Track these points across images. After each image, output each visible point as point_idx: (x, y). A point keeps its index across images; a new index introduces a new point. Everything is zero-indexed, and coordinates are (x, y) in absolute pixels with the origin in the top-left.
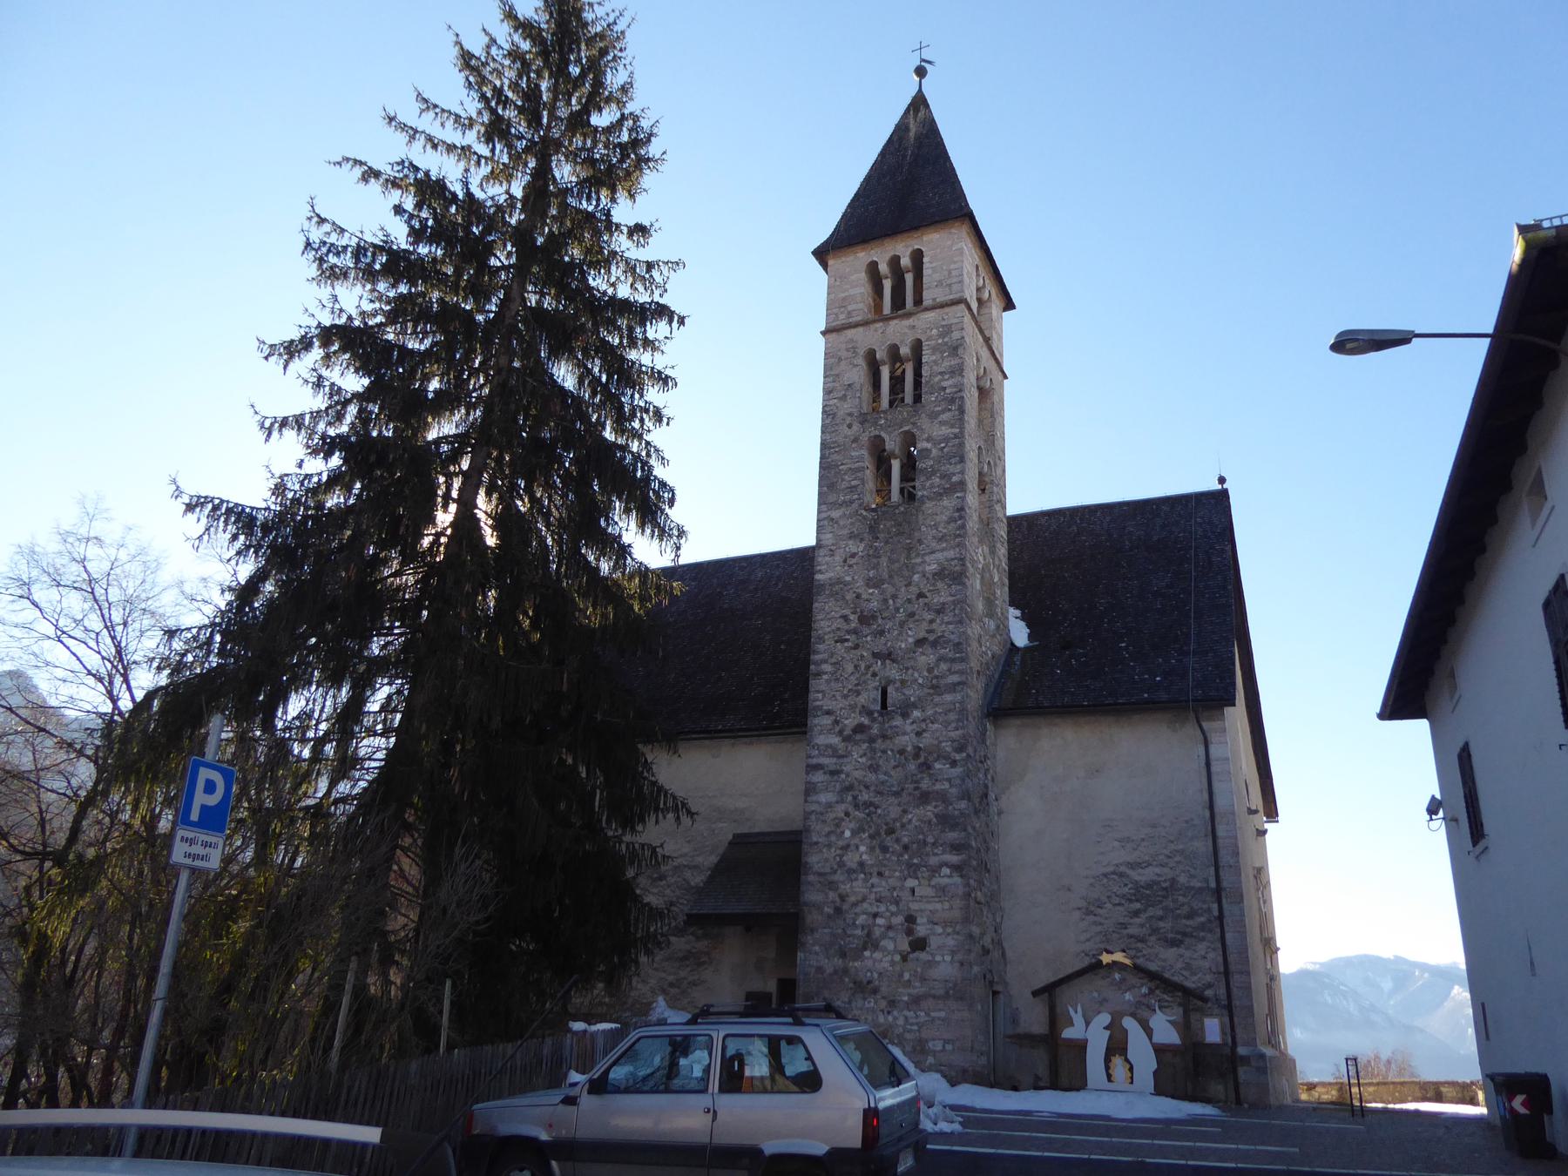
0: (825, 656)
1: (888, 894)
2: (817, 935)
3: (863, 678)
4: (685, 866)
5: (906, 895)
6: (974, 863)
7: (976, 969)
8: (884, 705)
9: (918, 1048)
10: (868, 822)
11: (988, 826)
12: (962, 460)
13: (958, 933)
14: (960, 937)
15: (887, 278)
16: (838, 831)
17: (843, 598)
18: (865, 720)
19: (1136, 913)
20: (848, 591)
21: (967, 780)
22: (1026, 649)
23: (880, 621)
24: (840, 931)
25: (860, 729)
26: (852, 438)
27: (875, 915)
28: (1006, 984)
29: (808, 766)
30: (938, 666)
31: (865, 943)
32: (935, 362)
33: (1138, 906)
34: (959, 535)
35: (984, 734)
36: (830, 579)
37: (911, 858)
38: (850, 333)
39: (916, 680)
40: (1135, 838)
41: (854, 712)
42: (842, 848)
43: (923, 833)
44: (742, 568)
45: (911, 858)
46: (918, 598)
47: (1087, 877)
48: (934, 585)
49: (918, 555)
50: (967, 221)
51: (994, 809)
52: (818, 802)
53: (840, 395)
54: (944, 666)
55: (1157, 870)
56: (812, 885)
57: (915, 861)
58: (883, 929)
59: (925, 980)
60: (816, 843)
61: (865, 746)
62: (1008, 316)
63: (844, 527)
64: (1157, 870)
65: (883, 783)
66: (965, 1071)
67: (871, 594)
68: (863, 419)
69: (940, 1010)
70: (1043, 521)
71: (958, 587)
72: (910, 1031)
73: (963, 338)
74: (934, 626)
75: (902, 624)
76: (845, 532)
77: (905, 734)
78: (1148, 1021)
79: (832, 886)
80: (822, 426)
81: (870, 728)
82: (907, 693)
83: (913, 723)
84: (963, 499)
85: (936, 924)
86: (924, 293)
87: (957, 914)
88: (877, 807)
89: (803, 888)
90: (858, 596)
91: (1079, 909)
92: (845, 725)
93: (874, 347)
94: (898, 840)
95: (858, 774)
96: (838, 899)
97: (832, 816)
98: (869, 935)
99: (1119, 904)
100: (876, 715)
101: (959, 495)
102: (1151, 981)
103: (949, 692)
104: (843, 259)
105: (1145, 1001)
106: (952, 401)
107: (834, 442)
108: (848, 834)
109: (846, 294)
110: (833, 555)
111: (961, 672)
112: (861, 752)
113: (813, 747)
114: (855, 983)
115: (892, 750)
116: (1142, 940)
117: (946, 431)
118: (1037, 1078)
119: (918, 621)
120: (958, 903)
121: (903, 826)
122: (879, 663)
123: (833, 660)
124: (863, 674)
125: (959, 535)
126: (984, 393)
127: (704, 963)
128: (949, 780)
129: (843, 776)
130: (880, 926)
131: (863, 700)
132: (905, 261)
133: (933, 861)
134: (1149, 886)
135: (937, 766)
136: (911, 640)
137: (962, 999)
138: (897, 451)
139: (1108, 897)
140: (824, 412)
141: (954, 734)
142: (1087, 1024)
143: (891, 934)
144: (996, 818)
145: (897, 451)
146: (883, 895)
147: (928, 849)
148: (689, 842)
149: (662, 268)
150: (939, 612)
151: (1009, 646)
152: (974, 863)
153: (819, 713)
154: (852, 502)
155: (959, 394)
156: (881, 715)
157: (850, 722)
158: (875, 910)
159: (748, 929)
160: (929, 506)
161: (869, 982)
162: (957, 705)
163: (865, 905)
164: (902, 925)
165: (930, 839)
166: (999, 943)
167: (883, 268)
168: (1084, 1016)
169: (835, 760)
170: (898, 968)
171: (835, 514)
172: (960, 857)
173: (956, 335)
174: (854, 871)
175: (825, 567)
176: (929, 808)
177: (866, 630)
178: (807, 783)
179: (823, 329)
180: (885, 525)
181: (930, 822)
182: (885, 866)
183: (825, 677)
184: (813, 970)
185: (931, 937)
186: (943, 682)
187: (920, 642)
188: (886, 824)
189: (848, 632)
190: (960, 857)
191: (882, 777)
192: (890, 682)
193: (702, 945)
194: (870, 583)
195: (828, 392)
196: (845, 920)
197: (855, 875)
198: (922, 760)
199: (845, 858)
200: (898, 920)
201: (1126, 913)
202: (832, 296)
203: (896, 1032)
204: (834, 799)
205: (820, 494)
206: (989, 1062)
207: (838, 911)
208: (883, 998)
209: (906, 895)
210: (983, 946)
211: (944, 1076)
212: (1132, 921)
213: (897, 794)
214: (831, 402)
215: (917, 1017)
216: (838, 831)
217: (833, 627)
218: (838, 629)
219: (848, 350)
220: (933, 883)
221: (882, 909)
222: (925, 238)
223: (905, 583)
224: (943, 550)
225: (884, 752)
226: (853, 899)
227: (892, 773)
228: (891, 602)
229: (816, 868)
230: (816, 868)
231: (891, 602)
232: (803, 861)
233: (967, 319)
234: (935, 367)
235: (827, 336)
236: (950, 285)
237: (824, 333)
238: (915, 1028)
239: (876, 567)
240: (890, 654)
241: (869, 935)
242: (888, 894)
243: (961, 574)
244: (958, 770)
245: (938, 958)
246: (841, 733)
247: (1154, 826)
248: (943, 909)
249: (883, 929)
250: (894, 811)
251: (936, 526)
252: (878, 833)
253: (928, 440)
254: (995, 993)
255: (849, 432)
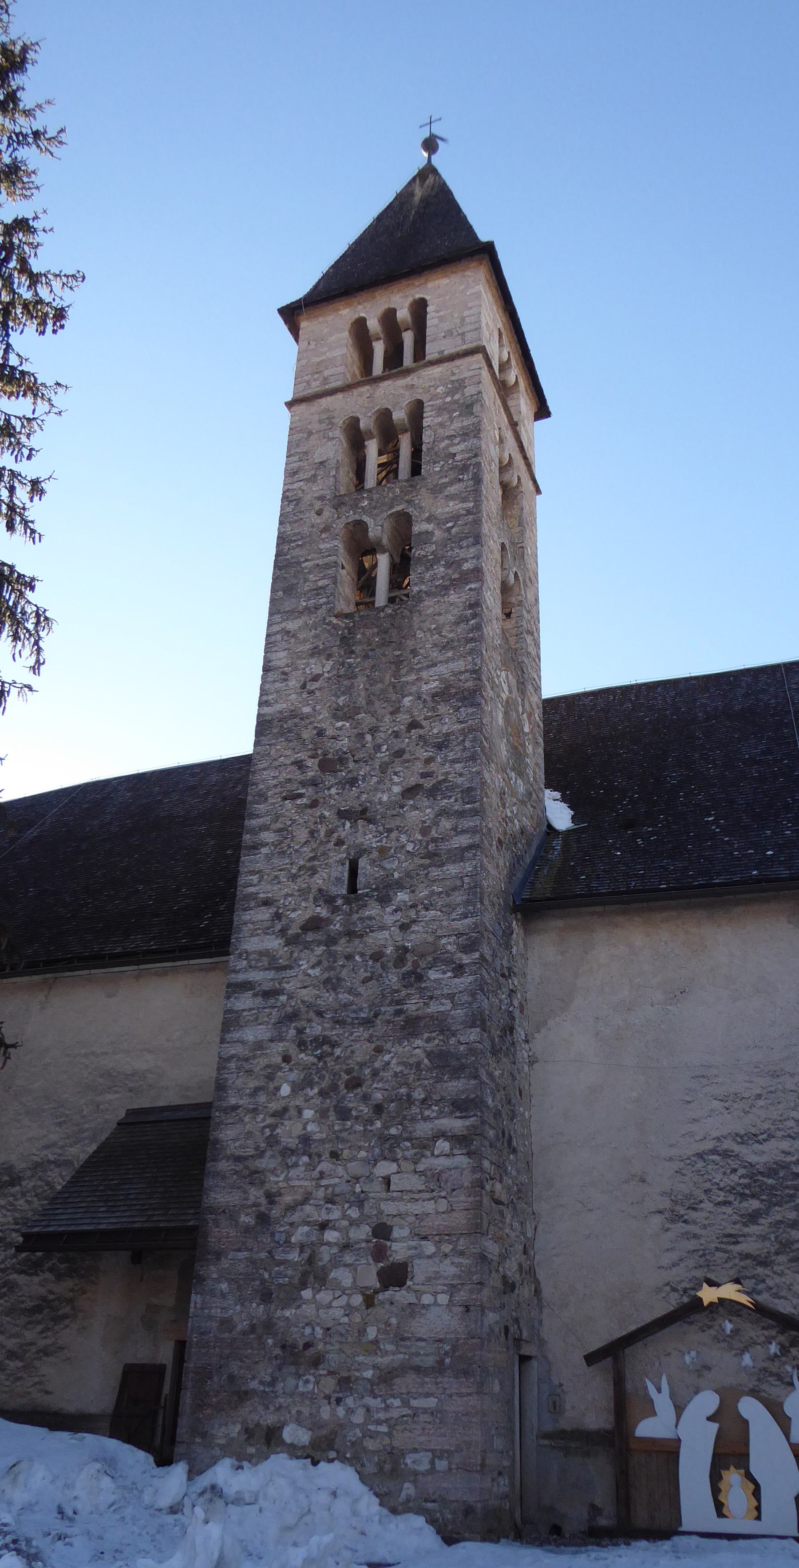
0: (266, 820)
1: (346, 1188)
2: (225, 1263)
3: (322, 849)
4: (49, 1162)
5: (376, 1189)
6: (491, 1133)
7: (492, 1317)
8: (353, 888)
9: (388, 1467)
10: (319, 1071)
11: (514, 1078)
12: (478, 540)
13: (462, 1254)
14: (465, 1261)
15: (378, 339)
16: (272, 1086)
17: (299, 737)
18: (323, 912)
19: (753, 1217)
20: (306, 727)
21: (480, 996)
22: (568, 832)
23: (351, 765)
24: (263, 1255)
25: (314, 924)
26: (322, 526)
27: (324, 1226)
28: (542, 1343)
29: (229, 985)
30: (436, 824)
31: (305, 1274)
32: (441, 425)
33: (755, 1204)
34: (472, 640)
35: (508, 933)
36: (281, 712)
37: (386, 1127)
38: (325, 402)
39: (403, 846)
40: (746, 1095)
41: (306, 900)
42: (274, 1115)
43: (407, 1084)
44: (193, 775)
45: (386, 1127)
46: (409, 730)
47: (671, 1159)
48: (434, 709)
49: (411, 670)
50: (486, 262)
51: (523, 1054)
52: (243, 1042)
53: (307, 475)
54: (446, 824)
55: (785, 1145)
56: (224, 1177)
57: (393, 1131)
58: (335, 1250)
59: (403, 1339)
60: (235, 1108)
61: (320, 950)
62: (538, 497)
63: (305, 640)
64: (785, 1145)
65: (345, 1006)
66: (468, 1510)
67: (340, 729)
68: (338, 503)
69: (428, 1395)
70: (587, 701)
71: (470, 710)
72: (373, 1435)
73: (480, 393)
74: (433, 767)
75: (384, 768)
76: (308, 646)
77: (382, 928)
78: (781, 1405)
79: (255, 1177)
80: (281, 515)
81: (328, 921)
82: (387, 866)
83: (396, 911)
84: (479, 591)
85: (425, 1238)
86: (428, 347)
87: (459, 1219)
88: (334, 1045)
89: (209, 1182)
90: (321, 733)
91: (660, 1212)
92: (292, 921)
93: (358, 415)
94: (366, 1098)
95: (306, 994)
96: (263, 1201)
97: (262, 1062)
98: (310, 1261)
99: (726, 1203)
100: (339, 902)
101: (473, 586)
102: (782, 1332)
103: (454, 862)
104: (321, 319)
105: (774, 1367)
106: (464, 469)
107: (295, 535)
108: (285, 1090)
109: (323, 357)
110: (286, 680)
111: (473, 831)
112: (314, 960)
113: (240, 955)
114: (283, 1347)
115: (362, 955)
116: (764, 1263)
117: (454, 506)
118: (270, 661)
119: (408, 761)
120: (462, 1199)
121: (375, 1073)
122: (348, 824)
123: (279, 825)
124: (321, 843)
125: (472, 640)
126: (509, 493)
127: (65, 1317)
128: (451, 997)
129: (283, 998)
130: (329, 1244)
131: (320, 882)
132: (403, 314)
133: (423, 1129)
134: (771, 1172)
135: (433, 975)
136: (397, 789)
137: (466, 1373)
138: (385, 541)
139: (707, 1191)
140: (285, 498)
141: (461, 925)
142: (679, 1410)
143: (348, 1258)
144: (526, 1068)
145: (385, 541)
146: (337, 1190)
147: (415, 1110)
148: (60, 1124)
149: (53, 283)
150: (440, 747)
151: (544, 828)
152: (491, 1133)
153: (252, 904)
154: (317, 608)
155: (474, 461)
156: (348, 901)
157: (298, 917)
158: (324, 1216)
159: (137, 1258)
160: (429, 605)
161: (307, 1346)
162: (466, 880)
163: (308, 1208)
164: (368, 1241)
165: (419, 1094)
166: (529, 1272)
167: (374, 325)
168: (672, 1396)
169: (271, 974)
170: (357, 1318)
171: (292, 625)
172: (468, 1122)
173: (470, 390)
174: (293, 1152)
175: (274, 696)
176: (419, 1042)
177: (330, 780)
178: (228, 1011)
179: (289, 398)
180: (363, 634)
181: (418, 1064)
182: (343, 1141)
183: (264, 850)
184: (215, 1325)
185: (417, 1261)
186: (444, 846)
187: (410, 792)
188: (349, 1072)
189: (303, 784)
190: (468, 1122)
191: (344, 997)
192: (362, 851)
193: (64, 1287)
194: (338, 713)
195: (291, 474)
196: (273, 1235)
197: (294, 1159)
198: (408, 967)
199: (278, 1131)
200: (362, 1232)
201: (736, 1217)
202: (304, 362)
203: (351, 1437)
204: (268, 1035)
205: (273, 601)
206: (512, 1484)
207: (263, 1219)
208: (331, 1373)
209: (376, 1189)
210: (504, 1277)
211: (431, 1521)
212: (746, 1230)
213: (368, 1023)
214: (295, 486)
215: (387, 1408)
216: (272, 1086)
217: (281, 779)
218: (289, 781)
219: (321, 422)
220: (421, 1167)
221: (336, 1214)
222: (430, 285)
223: (391, 709)
224: (447, 662)
225: (349, 957)
226: (288, 1199)
227: (361, 990)
228: (368, 737)
229: (233, 1148)
230: (233, 1148)
231: (368, 737)
232: (211, 1138)
233: (485, 374)
234: (440, 431)
235: (293, 409)
236: (463, 334)
237: (290, 405)
238: (384, 1429)
239: (348, 691)
240: (364, 811)
241: (310, 1261)
242: (346, 1188)
243: (475, 691)
244: (466, 980)
245: (427, 1299)
246: (283, 931)
247: (774, 1075)
248: (438, 1213)
249: (335, 1250)
250: (362, 1051)
251: (438, 630)
252: (334, 1087)
253: (429, 520)
254: (524, 1359)
255: (318, 520)
